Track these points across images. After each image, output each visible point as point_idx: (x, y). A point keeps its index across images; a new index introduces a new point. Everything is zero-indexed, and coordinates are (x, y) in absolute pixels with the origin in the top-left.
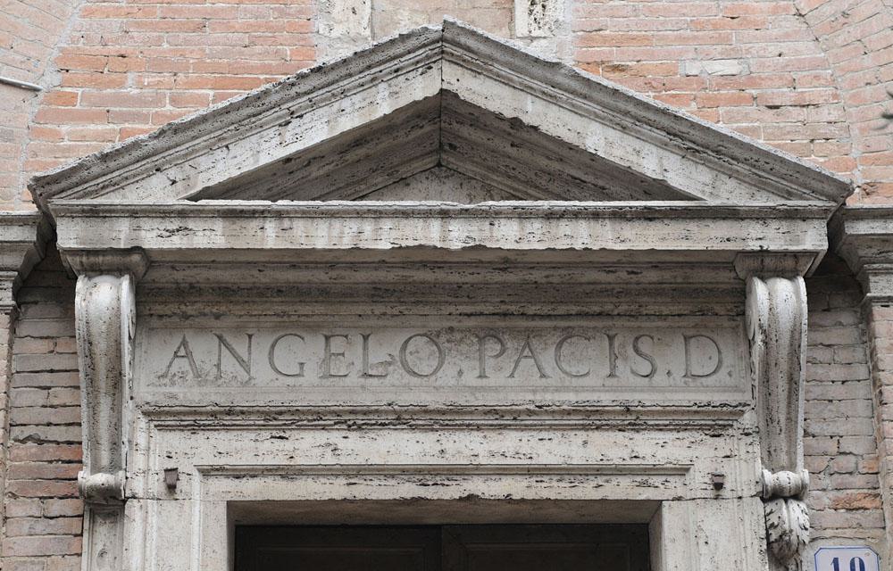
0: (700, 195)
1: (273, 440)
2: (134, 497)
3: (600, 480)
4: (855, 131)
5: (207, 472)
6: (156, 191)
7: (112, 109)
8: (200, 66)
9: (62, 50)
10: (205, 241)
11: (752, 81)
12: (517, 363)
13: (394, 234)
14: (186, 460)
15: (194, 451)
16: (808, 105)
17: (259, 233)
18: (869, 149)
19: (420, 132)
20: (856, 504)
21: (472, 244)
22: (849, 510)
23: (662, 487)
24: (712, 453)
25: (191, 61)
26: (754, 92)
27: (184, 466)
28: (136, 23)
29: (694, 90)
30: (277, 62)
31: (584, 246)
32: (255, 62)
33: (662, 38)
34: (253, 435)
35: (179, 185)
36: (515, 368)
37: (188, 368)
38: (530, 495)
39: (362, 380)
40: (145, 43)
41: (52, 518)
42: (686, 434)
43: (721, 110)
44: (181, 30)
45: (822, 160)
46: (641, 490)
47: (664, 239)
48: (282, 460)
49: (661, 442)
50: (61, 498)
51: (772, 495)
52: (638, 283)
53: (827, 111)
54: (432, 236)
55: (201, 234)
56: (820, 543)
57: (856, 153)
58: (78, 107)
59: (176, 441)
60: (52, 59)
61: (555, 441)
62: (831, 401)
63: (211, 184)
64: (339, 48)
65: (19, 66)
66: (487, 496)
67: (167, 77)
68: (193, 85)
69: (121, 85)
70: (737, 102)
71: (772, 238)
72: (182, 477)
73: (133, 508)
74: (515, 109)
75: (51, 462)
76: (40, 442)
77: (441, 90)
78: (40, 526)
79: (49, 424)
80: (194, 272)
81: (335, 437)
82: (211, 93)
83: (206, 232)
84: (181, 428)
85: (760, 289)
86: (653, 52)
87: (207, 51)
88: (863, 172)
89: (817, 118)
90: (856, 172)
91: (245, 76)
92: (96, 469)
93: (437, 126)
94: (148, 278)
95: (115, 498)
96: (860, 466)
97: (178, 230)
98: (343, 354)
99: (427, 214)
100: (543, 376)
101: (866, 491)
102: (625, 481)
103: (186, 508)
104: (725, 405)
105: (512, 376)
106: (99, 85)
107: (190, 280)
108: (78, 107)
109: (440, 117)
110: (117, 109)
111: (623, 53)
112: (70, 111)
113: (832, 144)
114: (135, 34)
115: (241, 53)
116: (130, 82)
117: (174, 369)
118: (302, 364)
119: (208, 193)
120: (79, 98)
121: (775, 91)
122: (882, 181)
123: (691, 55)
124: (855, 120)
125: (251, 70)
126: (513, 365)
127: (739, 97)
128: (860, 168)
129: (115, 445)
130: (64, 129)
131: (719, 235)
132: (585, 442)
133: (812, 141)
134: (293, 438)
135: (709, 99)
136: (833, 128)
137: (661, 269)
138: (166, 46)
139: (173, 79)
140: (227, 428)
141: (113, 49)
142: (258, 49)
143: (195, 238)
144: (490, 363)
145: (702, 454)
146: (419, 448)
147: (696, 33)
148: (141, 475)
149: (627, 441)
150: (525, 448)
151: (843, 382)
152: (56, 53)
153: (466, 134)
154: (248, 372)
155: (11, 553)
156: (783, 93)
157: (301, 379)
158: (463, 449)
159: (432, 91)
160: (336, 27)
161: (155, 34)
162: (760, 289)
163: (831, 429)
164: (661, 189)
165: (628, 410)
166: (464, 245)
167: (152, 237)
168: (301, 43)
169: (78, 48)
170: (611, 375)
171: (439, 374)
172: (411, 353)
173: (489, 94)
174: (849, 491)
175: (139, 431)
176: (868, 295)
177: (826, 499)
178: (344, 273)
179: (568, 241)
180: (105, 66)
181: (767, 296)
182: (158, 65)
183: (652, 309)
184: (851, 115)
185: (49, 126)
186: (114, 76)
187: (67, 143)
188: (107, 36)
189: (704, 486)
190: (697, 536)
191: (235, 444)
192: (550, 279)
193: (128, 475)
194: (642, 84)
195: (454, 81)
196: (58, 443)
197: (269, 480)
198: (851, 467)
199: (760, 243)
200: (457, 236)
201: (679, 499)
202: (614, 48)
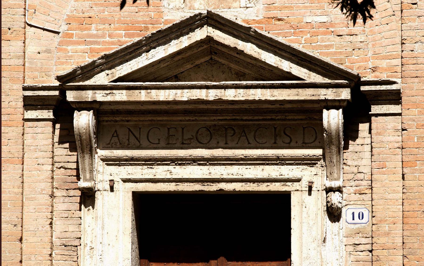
0: (303, 78)
1: (148, 169)
2: (98, 190)
3: (268, 184)
4: (370, 46)
5: (125, 181)
6: (102, 78)
7: (87, 39)
8: (119, 21)
9: (67, 15)
10: (119, 98)
11: (332, 24)
12: (239, 138)
13: (189, 94)
14: (117, 176)
15: (120, 173)
16: (353, 35)
17: (139, 94)
18: (375, 53)
19: (202, 48)
20: (363, 192)
21: (217, 98)
22: (360, 194)
23: (291, 186)
24: (310, 173)
25: (116, 19)
26: (333, 30)
27: (117, 179)
28: (95, 3)
29: (309, 29)
30: (149, 19)
31: (259, 99)
32: (140, 19)
33: (298, 7)
34: (141, 167)
35: (110, 76)
36: (239, 140)
37: (118, 141)
38: (242, 189)
39: (182, 145)
40: (98, 12)
41: (71, 197)
42: (300, 166)
43: (319, 37)
44: (112, 6)
45: (357, 58)
46: (283, 187)
47: (289, 95)
48: (151, 177)
49: (291, 169)
50: (74, 189)
51: (329, 190)
52: (284, 108)
53: (360, 37)
54: (202, 95)
55: (118, 95)
56: (348, 207)
57: (370, 54)
58: (74, 39)
59: (113, 169)
60: (64, 19)
61: (252, 169)
62: (356, 152)
63: (121, 75)
64: (172, 13)
65: (52, 22)
66: (226, 190)
67: (107, 26)
68: (116, 29)
69: (90, 29)
70: (325, 33)
71: (329, 94)
72: (115, 182)
73: (98, 194)
74: (235, 44)
75: (69, 176)
76: (66, 169)
77: (207, 36)
78: (67, 199)
79: (68, 162)
80: (118, 106)
81: (171, 168)
82: (124, 32)
83: (120, 94)
84: (116, 165)
85: (325, 112)
86: (294, 13)
87: (122, 15)
88: (372, 63)
89: (356, 40)
90: (369, 63)
91: (137, 25)
92: (86, 180)
93: (209, 45)
94: (101, 108)
95: (91, 191)
96: (365, 177)
97: (110, 94)
98: (174, 135)
99: (201, 87)
100: (249, 143)
101: (367, 187)
102: (278, 184)
103: (117, 194)
104: (315, 156)
105: (237, 143)
106: (82, 30)
107: (116, 108)
108: (74, 39)
109: (210, 42)
110: (89, 39)
111: (282, 13)
112: (71, 41)
113: (361, 51)
114: (95, 8)
115: (135, 15)
116: (93, 28)
117: (112, 141)
118: (159, 140)
119: (120, 79)
120: (74, 35)
121: (340, 29)
122: (379, 66)
123: (309, 14)
124: (370, 41)
125: (138, 22)
126: (238, 139)
127: (326, 32)
128: (371, 61)
129: (91, 171)
130: (69, 48)
131: (310, 94)
132: (263, 170)
133: (354, 50)
134: (155, 168)
135: (314, 32)
136: (362, 44)
137: (292, 103)
138: (106, 13)
139: (109, 26)
140: (131, 165)
141: (86, 15)
142: (141, 13)
143: (116, 97)
144: (229, 138)
145: (305, 173)
146: (202, 171)
147: (311, 5)
148: (101, 184)
149: (278, 169)
150: (240, 172)
151: (362, 145)
152: (65, 17)
153: (220, 49)
154: (139, 142)
155: (57, 209)
156: (344, 30)
157: (159, 145)
158: (218, 172)
159: (203, 36)
160: (171, 4)
161: (102, 8)
162: (325, 112)
163: (356, 163)
164: (289, 76)
165: (278, 158)
166: (215, 98)
167: (100, 96)
168: (158, 11)
169: (74, 15)
170: (275, 143)
171: (210, 143)
172: (200, 135)
173: (225, 38)
174: (360, 187)
175: (99, 165)
176: (370, 113)
177: (352, 190)
178: (172, 106)
179: (253, 96)
180: (83, 21)
181: (327, 117)
182: (103, 21)
183: (290, 117)
184: (369, 39)
185: (64, 47)
186: (87, 26)
187: (70, 54)
188: (84, 9)
189: (306, 186)
190: (302, 204)
191: (135, 171)
192: (250, 107)
193: (96, 182)
194: (289, 26)
195: (212, 32)
196: (72, 169)
197: (147, 183)
198: (362, 178)
199: (325, 96)
200: (212, 95)
201: (298, 190)
202: (279, 11)
